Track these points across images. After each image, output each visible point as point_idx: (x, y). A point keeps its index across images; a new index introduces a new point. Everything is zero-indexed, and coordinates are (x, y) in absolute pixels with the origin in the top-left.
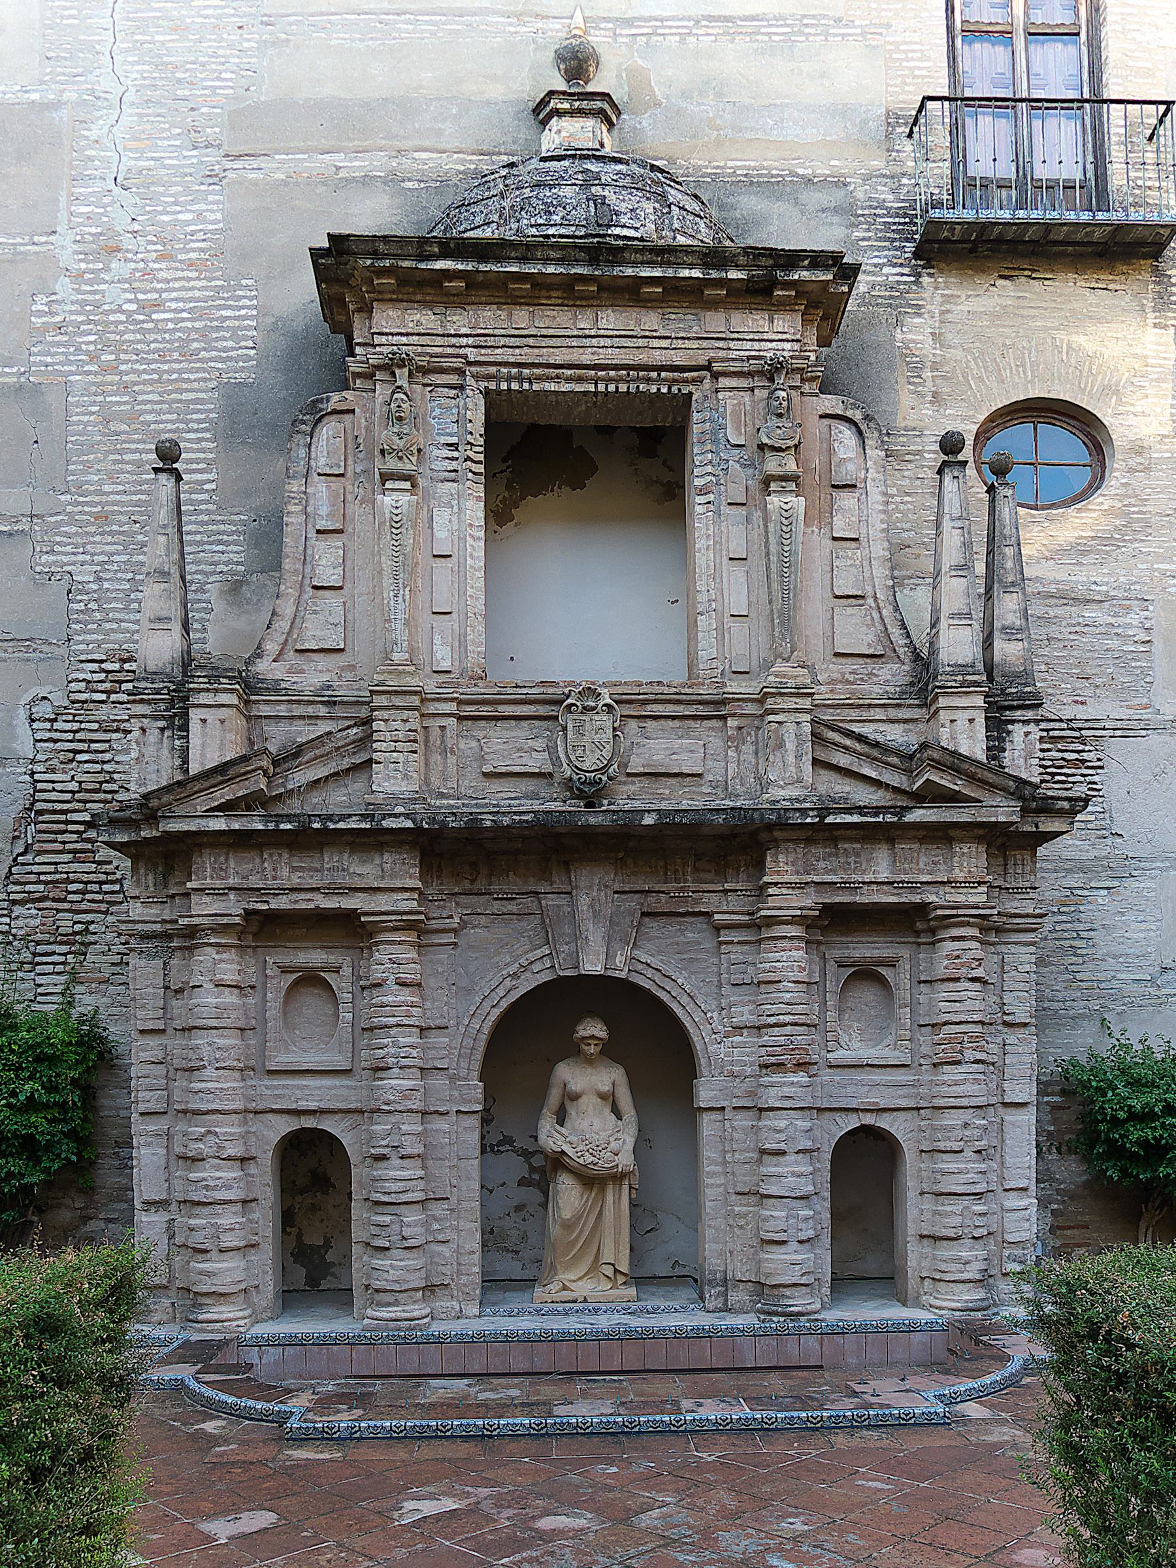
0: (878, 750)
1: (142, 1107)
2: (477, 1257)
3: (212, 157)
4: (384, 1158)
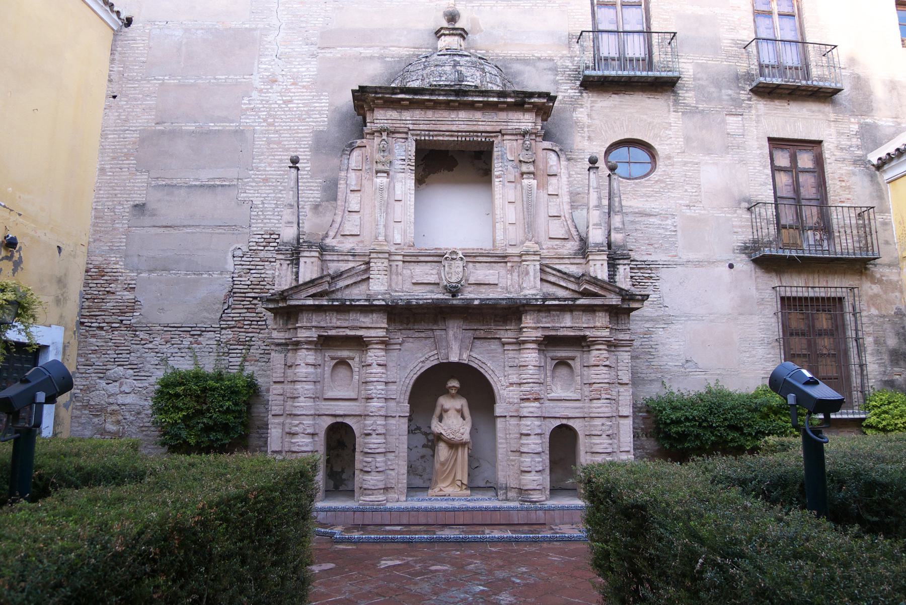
0: (566, 275)
1: (273, 413)
2: (405, 476)
3: (313, 49)
4: (370, 434)
